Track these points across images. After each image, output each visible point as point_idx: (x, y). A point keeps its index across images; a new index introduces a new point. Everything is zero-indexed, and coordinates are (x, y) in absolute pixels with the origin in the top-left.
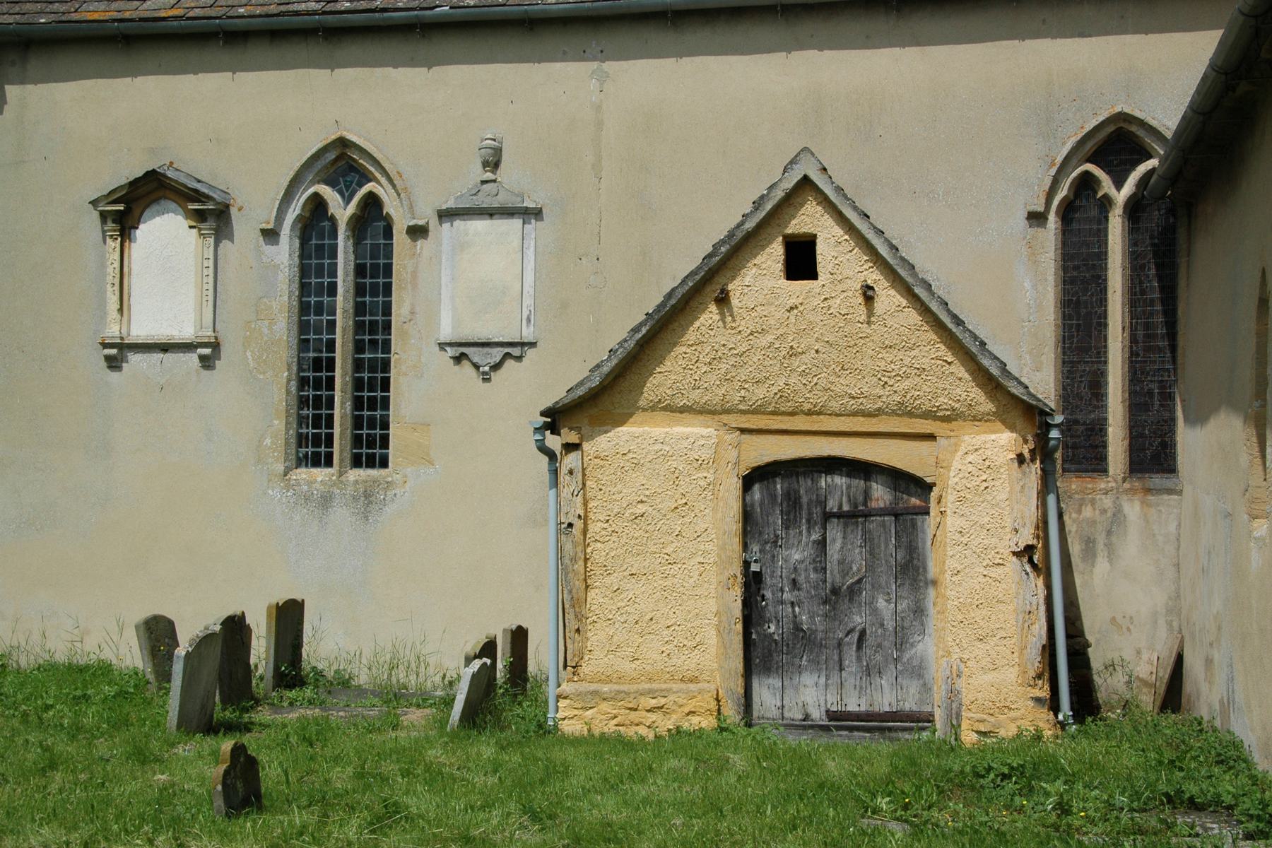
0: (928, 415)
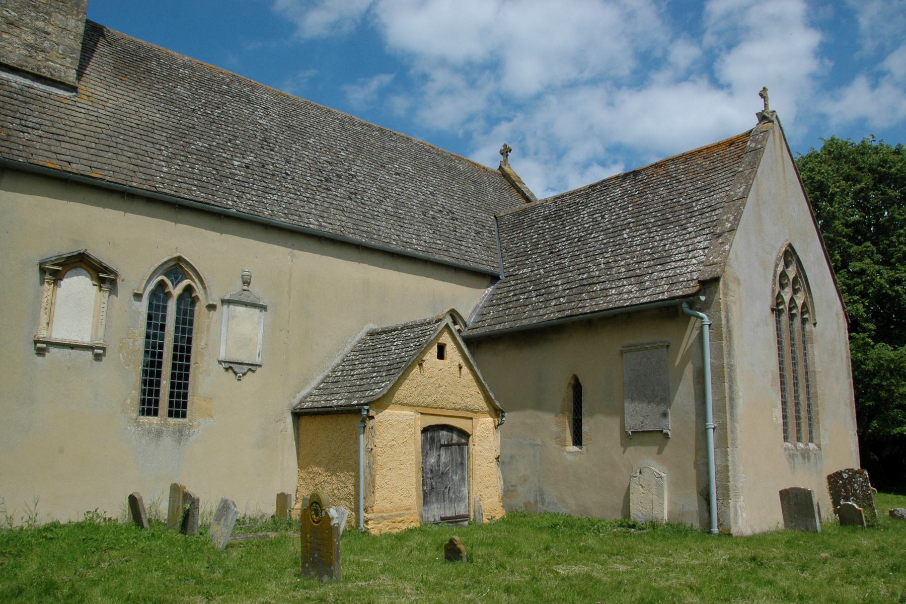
0: (472, 411)
